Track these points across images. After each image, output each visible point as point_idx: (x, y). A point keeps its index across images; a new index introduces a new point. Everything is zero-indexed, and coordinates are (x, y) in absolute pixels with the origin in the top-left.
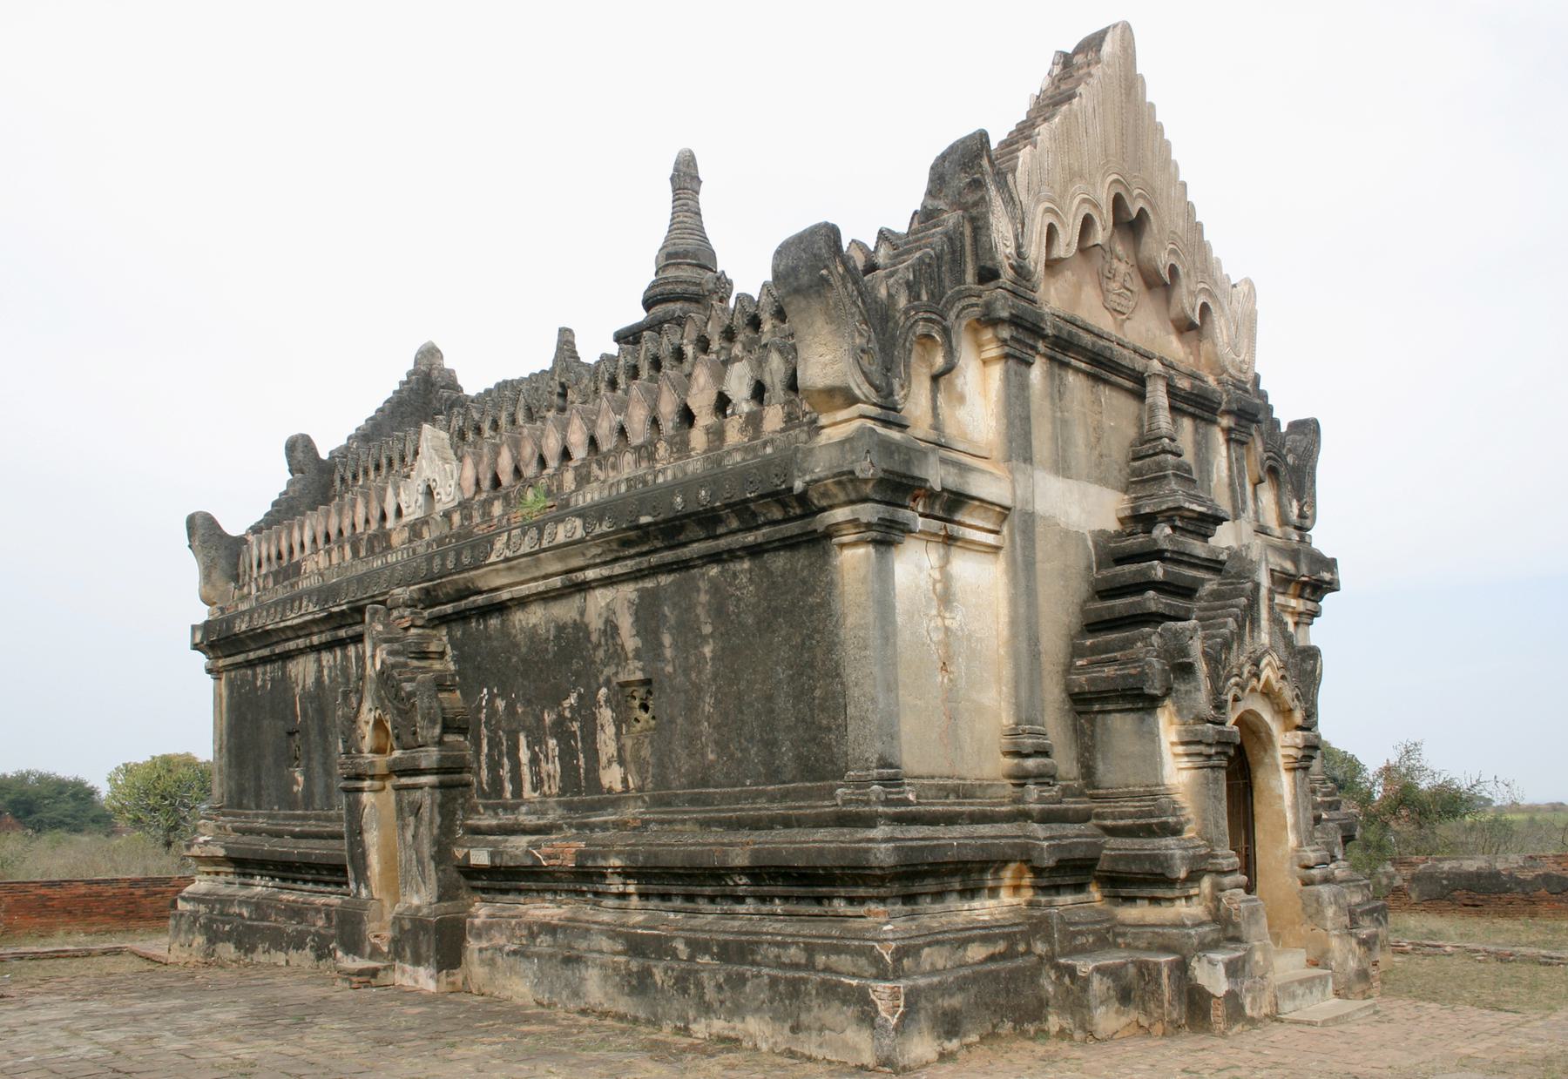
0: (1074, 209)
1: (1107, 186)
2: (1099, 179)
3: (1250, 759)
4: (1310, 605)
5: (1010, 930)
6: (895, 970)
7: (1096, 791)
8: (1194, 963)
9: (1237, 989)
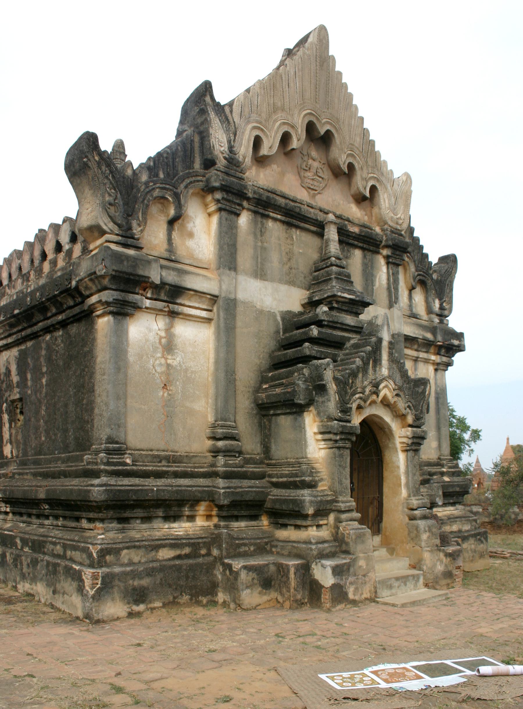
0: (276, 127)
1: (302, 116)
2: (296, 112)
3: (381, 445)
4: (445, 359)
5: (196, 541)
6: (99, 562)
7: (270, 461)
8: (313, 566)
9: (342, 583)
